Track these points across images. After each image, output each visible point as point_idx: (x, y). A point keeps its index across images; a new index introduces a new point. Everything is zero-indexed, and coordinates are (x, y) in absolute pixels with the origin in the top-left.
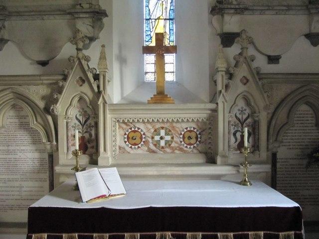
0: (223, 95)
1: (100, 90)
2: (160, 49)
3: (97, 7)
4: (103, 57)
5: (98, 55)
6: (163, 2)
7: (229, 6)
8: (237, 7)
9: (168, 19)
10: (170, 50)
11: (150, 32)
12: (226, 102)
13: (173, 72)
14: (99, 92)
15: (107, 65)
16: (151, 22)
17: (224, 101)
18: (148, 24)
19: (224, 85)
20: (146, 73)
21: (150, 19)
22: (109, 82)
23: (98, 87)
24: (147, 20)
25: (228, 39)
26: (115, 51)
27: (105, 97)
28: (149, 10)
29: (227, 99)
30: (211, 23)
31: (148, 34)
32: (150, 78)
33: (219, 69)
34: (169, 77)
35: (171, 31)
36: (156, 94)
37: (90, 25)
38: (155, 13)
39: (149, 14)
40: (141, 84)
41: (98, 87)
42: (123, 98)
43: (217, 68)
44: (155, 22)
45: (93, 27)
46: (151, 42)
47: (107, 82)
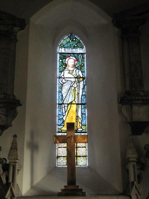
0: (136, 187)
1: (9, 182)
2: (70, 137)
3: (11, 97)
4: (14, 147)
5: (9, 146)
6: (75, 88)
7: (137, 98)
8: (144, 98)
9: (80, 104)
10: (76, 156)
11: (62, 116)
12: (140, 194)
13: (86, 156)
14: (8, 184)
15: (17, 156)
16: (63, 106)
17: (137, 194)
18: (61, 108)
19: (136, 175)
20: (58, 157)
21: (63, 104)
22: (18, 170)
23: (7, 178)
24: (59, 104)
25: (137, 128)
26: (27, 138)
27: (13, 189)
28: (62, 95)
29: (141, 191)
30: (120, 111)
31: (61, 118)
32: (62, 162)
33: (130, 160)
34: (82, 162)
35: (83, 115)
36: (67, 185)
37: (4, 115)
38: (67, 98)
39: (62, 99)
40: (53, 170)
41: (7, 178)
42: (32, 187)
43: (128, 159)
44: (67, 106)
45: (6, 116)
46: (64, 126)
47: (17, 171)
